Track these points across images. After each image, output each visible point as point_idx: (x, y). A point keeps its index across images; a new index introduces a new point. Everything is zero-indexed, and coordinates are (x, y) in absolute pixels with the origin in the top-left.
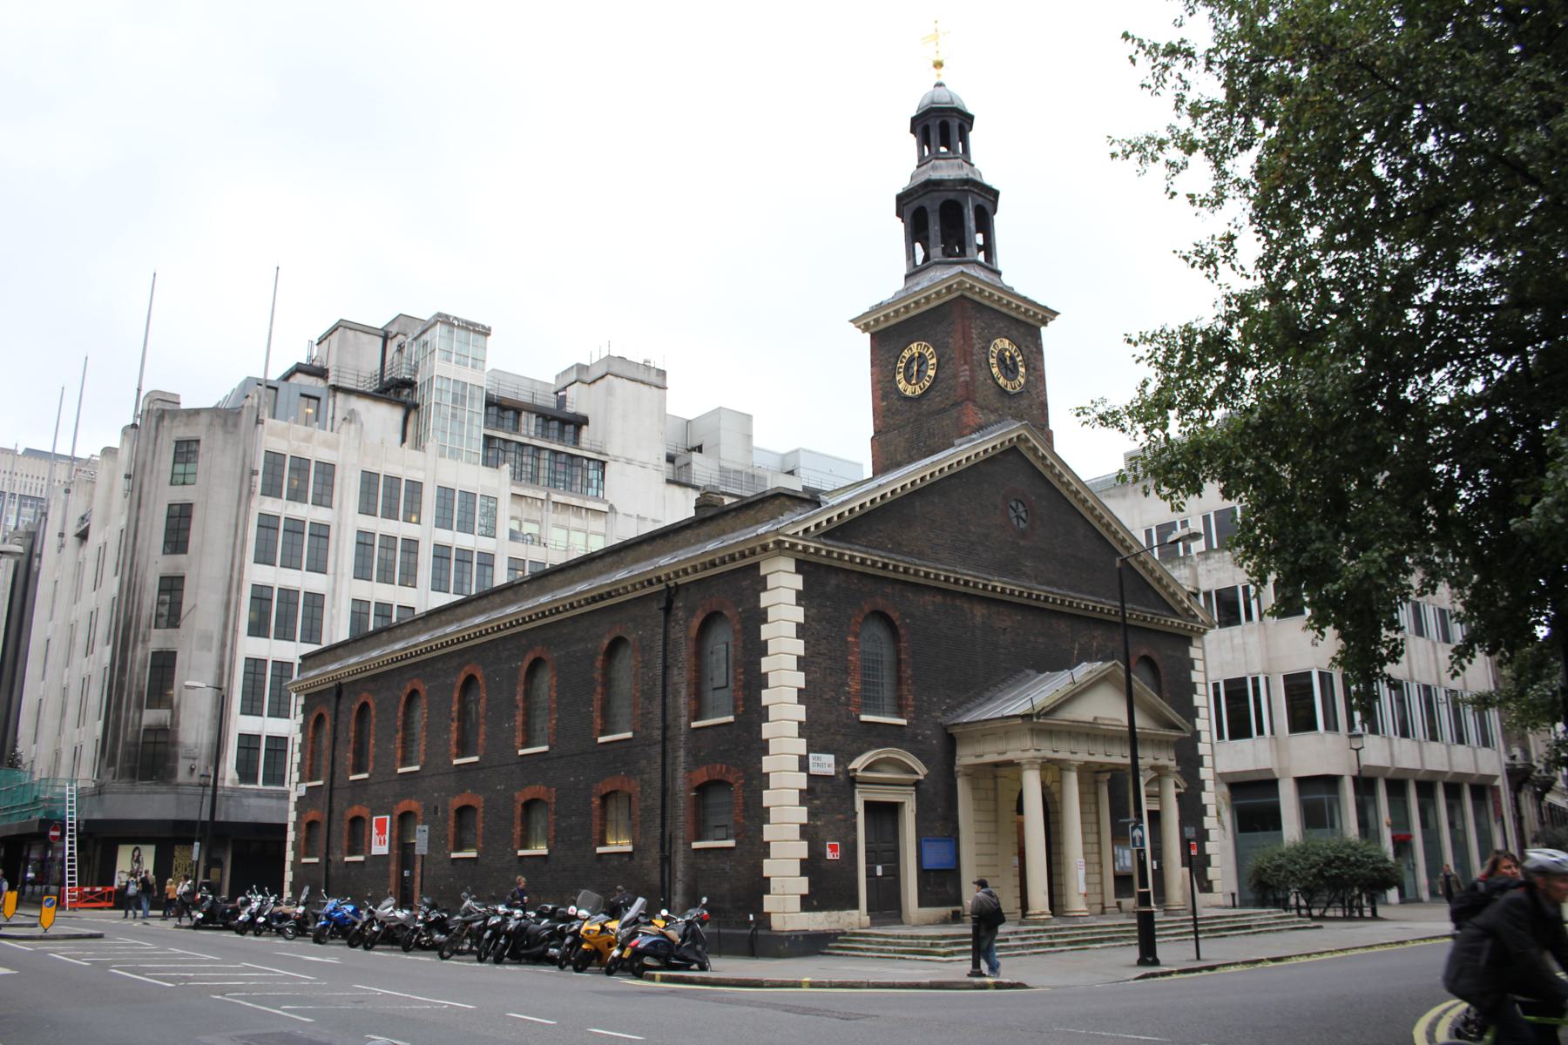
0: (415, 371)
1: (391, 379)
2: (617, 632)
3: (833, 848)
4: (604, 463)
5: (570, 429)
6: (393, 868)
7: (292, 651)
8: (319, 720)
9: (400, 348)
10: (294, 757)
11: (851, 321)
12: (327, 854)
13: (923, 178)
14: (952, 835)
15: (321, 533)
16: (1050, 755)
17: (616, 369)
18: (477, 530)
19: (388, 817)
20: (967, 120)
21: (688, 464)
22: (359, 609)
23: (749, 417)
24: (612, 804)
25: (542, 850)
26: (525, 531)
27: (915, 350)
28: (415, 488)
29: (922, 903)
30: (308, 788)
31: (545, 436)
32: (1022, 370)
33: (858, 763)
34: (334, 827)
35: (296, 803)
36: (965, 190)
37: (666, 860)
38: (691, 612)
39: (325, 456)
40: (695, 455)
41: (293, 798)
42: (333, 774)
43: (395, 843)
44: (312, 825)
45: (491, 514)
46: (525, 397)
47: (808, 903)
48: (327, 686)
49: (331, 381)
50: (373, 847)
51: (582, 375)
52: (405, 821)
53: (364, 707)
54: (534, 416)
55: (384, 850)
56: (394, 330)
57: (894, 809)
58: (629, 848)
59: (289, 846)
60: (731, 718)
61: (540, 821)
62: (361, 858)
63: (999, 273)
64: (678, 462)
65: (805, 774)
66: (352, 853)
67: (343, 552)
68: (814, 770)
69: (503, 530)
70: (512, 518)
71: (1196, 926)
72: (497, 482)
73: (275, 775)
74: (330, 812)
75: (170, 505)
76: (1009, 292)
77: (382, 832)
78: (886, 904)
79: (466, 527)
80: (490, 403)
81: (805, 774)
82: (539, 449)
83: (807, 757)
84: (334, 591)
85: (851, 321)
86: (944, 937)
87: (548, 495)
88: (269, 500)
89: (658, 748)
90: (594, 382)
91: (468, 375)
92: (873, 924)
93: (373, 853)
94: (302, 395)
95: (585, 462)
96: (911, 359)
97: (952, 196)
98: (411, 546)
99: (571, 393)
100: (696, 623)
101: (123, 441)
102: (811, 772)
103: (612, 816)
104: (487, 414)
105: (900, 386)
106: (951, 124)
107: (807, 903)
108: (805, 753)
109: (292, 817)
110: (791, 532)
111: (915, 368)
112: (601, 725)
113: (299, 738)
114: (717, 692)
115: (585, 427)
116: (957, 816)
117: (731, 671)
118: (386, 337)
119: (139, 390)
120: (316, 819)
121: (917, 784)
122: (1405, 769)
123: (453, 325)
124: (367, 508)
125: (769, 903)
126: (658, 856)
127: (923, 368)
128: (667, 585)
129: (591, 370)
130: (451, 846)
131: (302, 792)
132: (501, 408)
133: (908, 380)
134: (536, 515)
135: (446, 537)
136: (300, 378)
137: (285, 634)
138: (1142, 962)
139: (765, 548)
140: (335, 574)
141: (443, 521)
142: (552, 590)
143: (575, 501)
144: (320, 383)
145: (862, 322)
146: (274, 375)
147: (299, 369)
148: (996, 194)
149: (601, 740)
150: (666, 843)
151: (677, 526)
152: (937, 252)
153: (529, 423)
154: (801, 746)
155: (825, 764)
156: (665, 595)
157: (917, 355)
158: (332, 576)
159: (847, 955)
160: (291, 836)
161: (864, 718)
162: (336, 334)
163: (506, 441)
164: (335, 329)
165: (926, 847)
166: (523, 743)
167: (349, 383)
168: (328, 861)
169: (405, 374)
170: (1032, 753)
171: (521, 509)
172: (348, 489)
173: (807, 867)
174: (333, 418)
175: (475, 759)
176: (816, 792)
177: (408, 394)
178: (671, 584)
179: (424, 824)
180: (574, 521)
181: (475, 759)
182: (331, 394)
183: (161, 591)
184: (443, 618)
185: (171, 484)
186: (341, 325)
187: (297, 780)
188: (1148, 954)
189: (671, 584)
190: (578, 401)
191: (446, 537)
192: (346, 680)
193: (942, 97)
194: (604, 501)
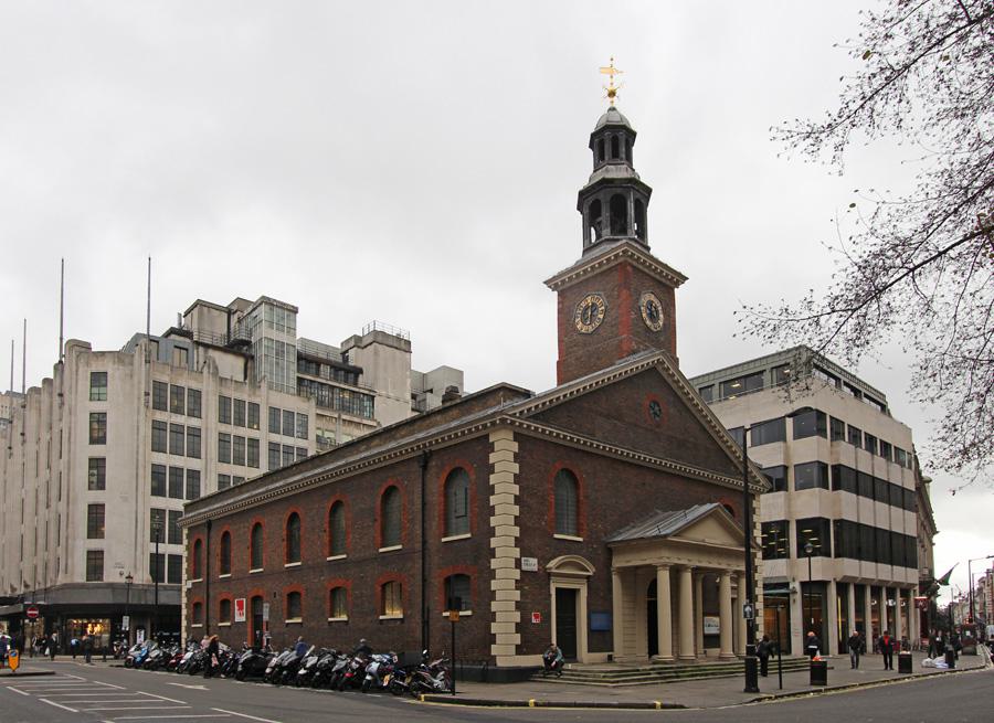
3: (536, 617)
4: (373, 397)
6: (249, 630)
7: (178, 504)
8: (198, 543)
9: (239, 321)
11: (545, 283)
12: (207, 621)
13: (600, 175)
14: (609, 612)
15: (195, 433)
16: (677, 562)
17: (380, 339)
20: (631, 135)
21: (425, 400)
22: (223, 479)
23: (461, 372)
24: (388, 590)
25: (344, 618)
26: (326, 436)
28: (255, 407)
31: (336, 380)
32: (661, 316)
33: (552, 564)
34: (211, 605)
37: (426, 623)
39: (195, 386)
40: (429, 394)
41: (184, 589)
42: (208, 574)
43: (250, 615)
44: (197, 606)
45: (305, 425)
46: (322, 355)
51: (357, 342)
52: (256, 601)
53: (226, 535)
55: (243, 619)
56: (234, 308)
57: (573, 593)
58: (401, 616)
59: (183, 618)
60: (469, 535)
63: (648, 249)
64: (418, 399)
65: (518, 571)
67: (210, 445)
68: (524, 568)
69: (312, 436)
70: (318, 429)
71: (780, 665)
72: (307, 407)
73: (175, 577)
75: (91, 414)
76: (546, 395)
77: (241, 608)
78: (570, 651)
79: (289, 432)
80: (300, 357)
81: (518, 571)
82: (334, 387)
83: (520, 560)
84: (206, 469)
85: (545, 283)
86: (611, 672)
88: (158, 412)
90: (366, 347)
91: (284, 338)
94: (176, 347)
96: (586, 309)
97: (619, 191)
98: (254, 443)
99: (351, 353)
101: (55, 376)
103: (389, 596)
104: (298, 365)
106: (620, 137)
107: (520, 650)
109: (184, 600)
116: (611, 599)
117: (469, 506)
118: (229, 312)
119: (61, 339)
121: (588, 577)
122: (849, 577)
123: (272, 305)
124: (224, 419)
125: (494, 650)
126: (420, 621)
127: (595, 313)
129: (364, 339)
130: (285, 616)
132: (309, 361)
134: (331, 427)
135: (276, 438)
136: (173, 336)
137: (175, 494)
138: (747, 690)
139: (493, 424)
141: (274, 429)
142: (344, 457)
143: (356, 420)
144: (188, 340)
145: (552, 283)
146: (158, 331)
147: (172, 331)
148: (649, 191)
149: (381, 550)
150: (425, 612)
152: (606, 233)
153: (325, 370)
154: (517, 552)
155: (532, 564)
158: (204, 461)
160: (184, 612)
161: (556, 536)
162: (196, 309)
163: (311, 381)
164: (195, 306)
165: (594, 617)
167: (207, 341)
168: (208, 626)
171: (323, 423)
172: (210, 406)
173: (519, 628)
175: (299, 563)
176: (525, 580)
181: (299, 563)
183: (90, 468)
185: (91, 400)
186: (199, 304)
188: (751, 686)
190: (355, 359)
191: (276, 438)
193: (615, 119)
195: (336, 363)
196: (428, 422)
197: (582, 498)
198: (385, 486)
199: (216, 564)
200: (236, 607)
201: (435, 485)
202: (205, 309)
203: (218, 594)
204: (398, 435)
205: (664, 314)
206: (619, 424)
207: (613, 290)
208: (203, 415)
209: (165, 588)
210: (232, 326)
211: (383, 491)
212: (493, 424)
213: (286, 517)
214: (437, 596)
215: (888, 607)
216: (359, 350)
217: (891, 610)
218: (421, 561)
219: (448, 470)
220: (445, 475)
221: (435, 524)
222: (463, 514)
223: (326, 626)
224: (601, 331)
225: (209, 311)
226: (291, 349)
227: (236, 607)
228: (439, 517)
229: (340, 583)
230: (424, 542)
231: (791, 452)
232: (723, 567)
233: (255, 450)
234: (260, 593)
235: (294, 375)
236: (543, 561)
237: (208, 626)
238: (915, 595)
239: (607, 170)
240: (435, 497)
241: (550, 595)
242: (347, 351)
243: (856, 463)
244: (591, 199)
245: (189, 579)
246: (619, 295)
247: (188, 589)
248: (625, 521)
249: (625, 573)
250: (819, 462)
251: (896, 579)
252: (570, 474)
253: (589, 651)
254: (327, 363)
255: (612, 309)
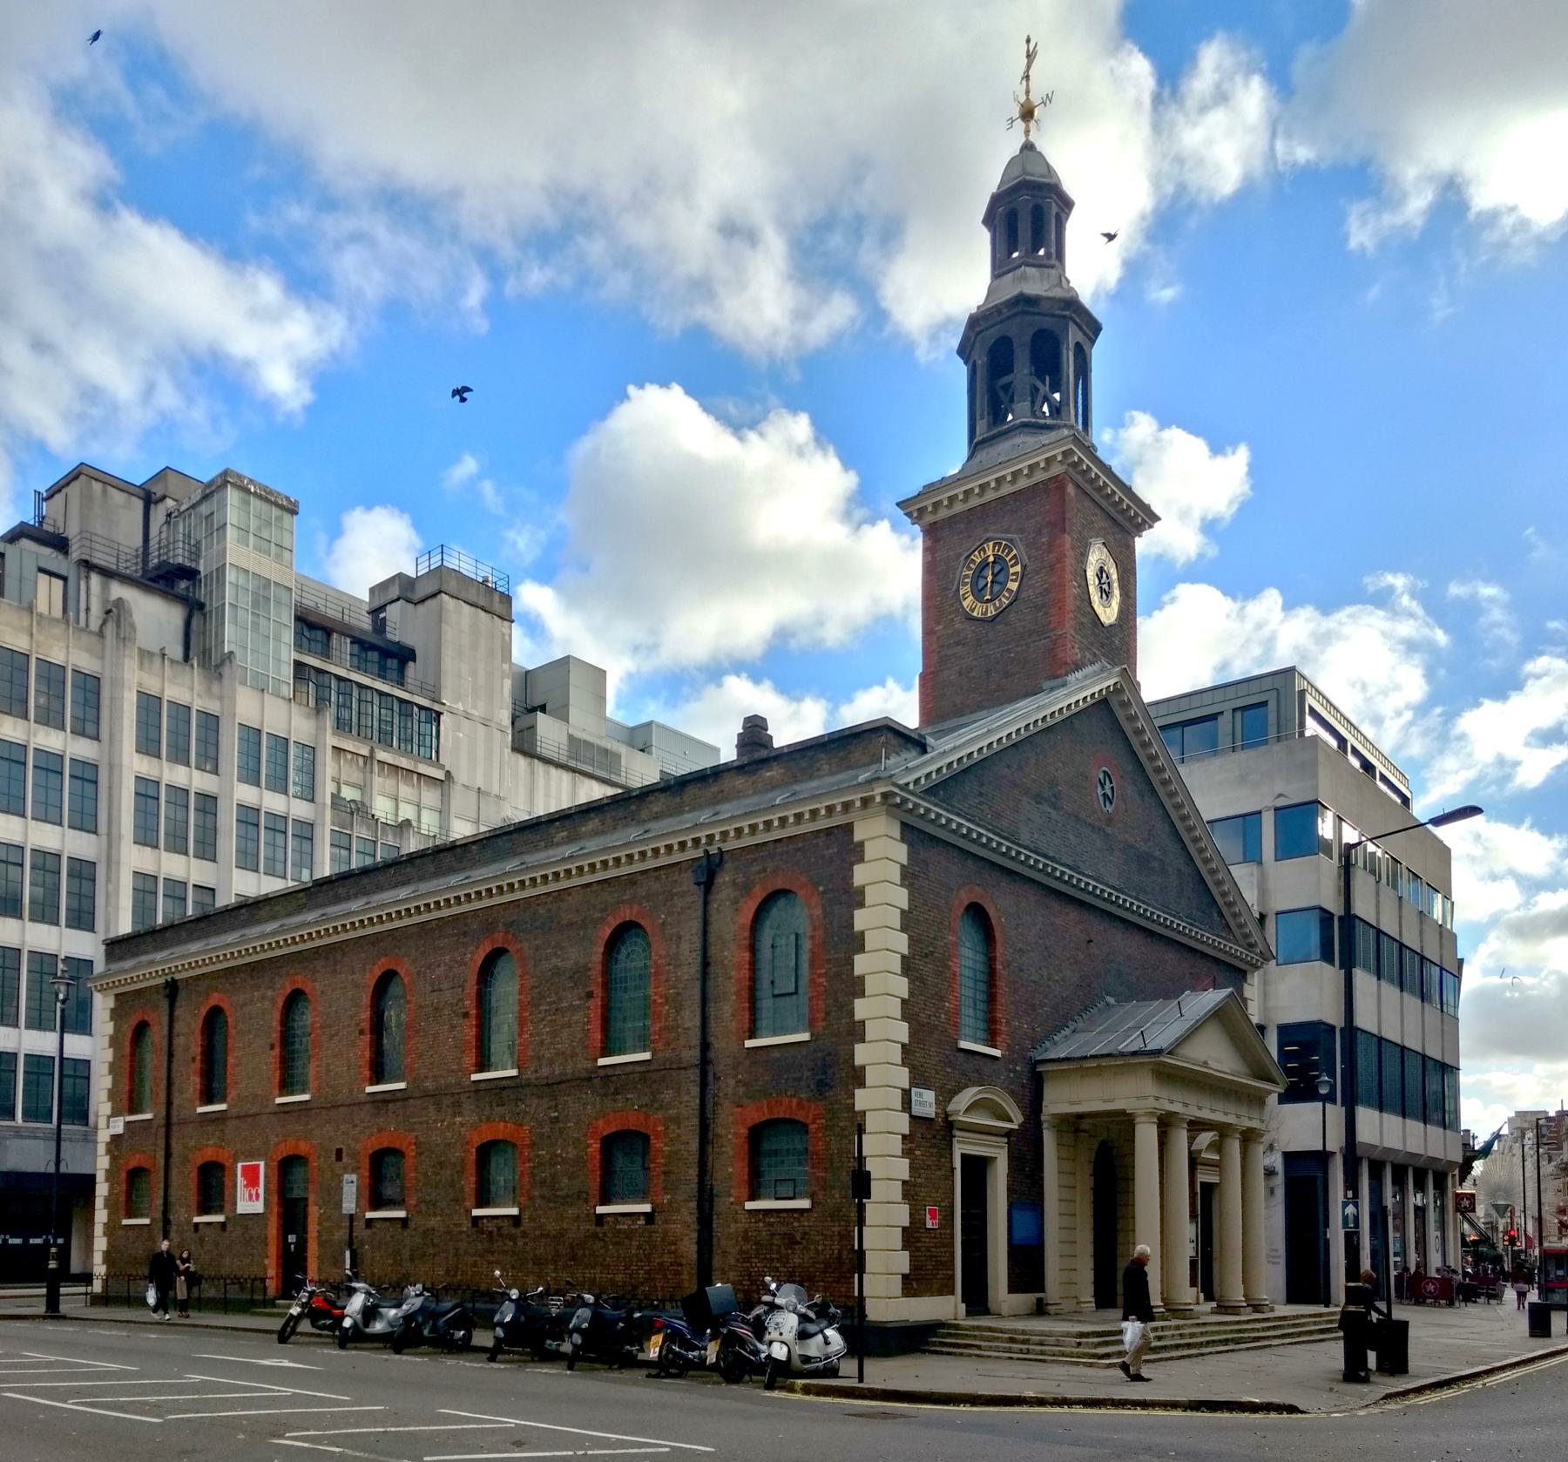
0: (196, 553)
1: (163, 564)
2: (627, 914)
4: (439, 714)
5: (392, 663)
6: (273, 1231)
8: (141, 1029)
10: (101, 1084)
11: (898, 504)
12: (165, 1212)
13: (1010, 290)
18: (292, 789)
19: (262, 1164)
21: (533, 727)
22: (145, 885)
27: (990, 552)
28: (211, 723)
29: (1013, 1288)
30: (127, 1124)
31: (361, 667)
35: (107, 1144)
36: (1064, 317)
38: (746, 889)
41: (104, 1136)
42: (169, 1103)
43: (275, 1198)
44: (135, 1176)
46: (332, 612)
47: (913, 1284)
48: (152, 983)
49: (75, 554)
50: (239, 1204)
54: (348, 641)
55: (258, 1207)
60: (805, 1037)
61: (502, 1173)
62: (220, 1218)
66: (205, 1209)
69: (327, 789)
73: (77, 1109)
74: (168, 1155)
77: (251, 1176)
85: (898, 504)
87: (372, 751)
89: (694, 1074)
90: (423, 601)
92: (969, 1313)
93: (239, 1211)
95: (416, 709)
96: (984, 565)
97: (1047, 323)
98: (208, 803)
99: (393, 613)
100: (746, 916)
102: (913, 1114)
105: (965, 604)
108: (907, 1087)
109: (103, 1162)
110: (902, 782)
111: (990, 578)
112: (602, 1041)
113: (108, 1055)
114: (781, 1001)
115: (411, 664)
118: (149, 498)
120: (145, 1165)
121: (1009, 1134)
123: (248, 491)
128: (706, 852)
131: (118, 1126)
133: (978, 593)
140: (109, 835)
143: (404, 762)
149: (602, 1062)
151: (847, 733)
154: (902, 1077)
156: (704, 862)
157: (991, 559)
158: (104, 838)
159: (961, 1354)
160: (102, 1189)
162: (76, 485)
165: (1016, 1215)
166: (476, 1065)
168: (166, 1222)
169: (180, 558)
170: (1151, 1103)
174: (88, 609)
177: (188, 588)
178: (713, 850)
179: (353, 1171)
180: (405, 791)
182: (83, 574)
184: (341, 891)
187: (109, 1112)
189: (713, 850)
190: (402, 625)
192: (185, 975)
194: (437, 764)
195: (363, 631)
196: (714, 789)
197: (999, 967)
198: (613, 922)
199: (190, 1081)
200: (240, 1181)
201: (731, 921)
202: (97, 487)
203: (193, 1149)
204: (644, 814)
205: (1121, 587)
206: (1054, 814)
207: (1039, 533)
208: (104, 733)
209: (18, 1133)
210: (154, 531)
211: (608, 931)
212: (866, 802)
213: (370, 979)
214: (730, 1165)
215: (1417, 1208)
216: (410, 606)
217: (1421, 1212)
218: (695, 1091)
219: (759, 894)
220: (753, 905)
221: (728, 1011)
222: (792, 989)
223: (466, 1226)
224: (1012, 617)
225: (104, 492)
226: (284, 595)
227: (240, 1181)
228: (738, 993)
229: (501, 1130)
230: (705, 1046)
231: (1271, 885)
232: (1230, 1119)
233: (210, 818)
234: (303, 1148)
235: (289, 654)
236: (945, 1096)
237: (166, 1222)
238: (1454, 1186)
239: (1024, 278)
240: (730, 955)
241: (953, 1169)
242: (382, 608)
243: (1378, 913)
244: (993, 334)
245: (116, 1113)
246: (1050, 544)
247: (116, 1139)
248: (1061, 1020)
249: (1073, 1124)
250: (1321, 909)
251: (1431, 1154)
252: (977, 913)
253: (1010, 1291)
254: (346, 631)
255: (1037, 572)
